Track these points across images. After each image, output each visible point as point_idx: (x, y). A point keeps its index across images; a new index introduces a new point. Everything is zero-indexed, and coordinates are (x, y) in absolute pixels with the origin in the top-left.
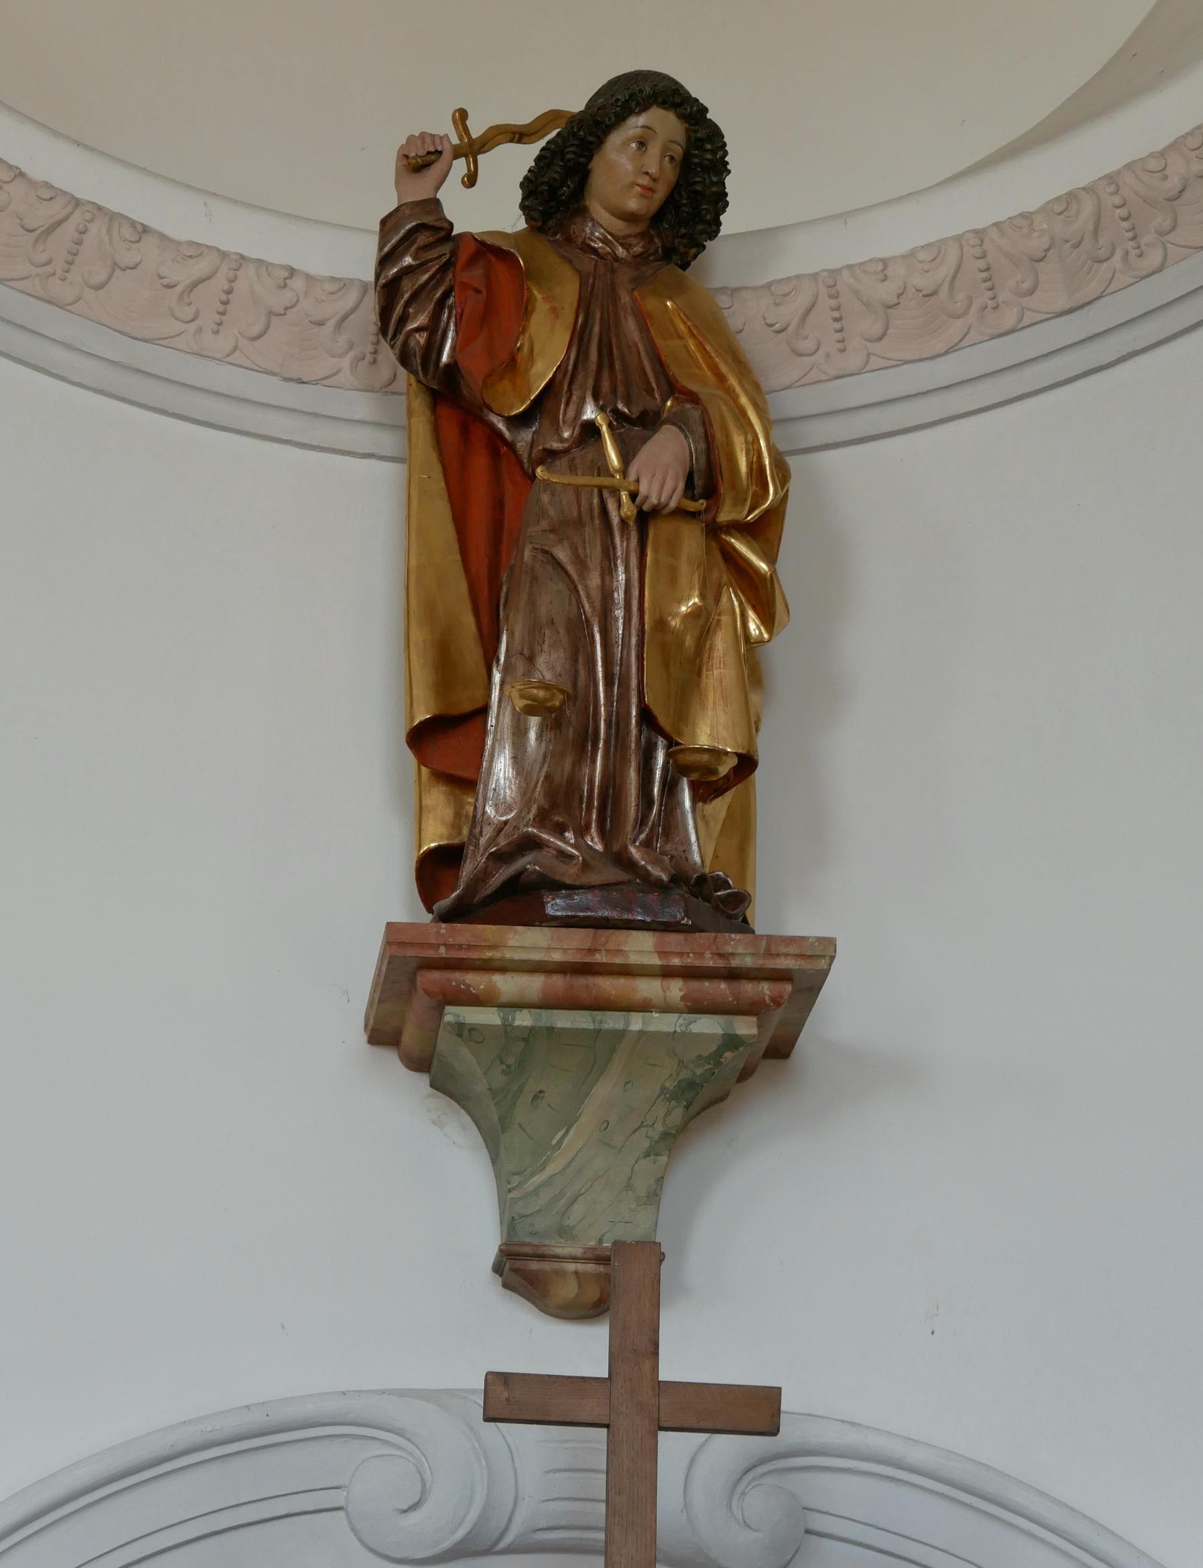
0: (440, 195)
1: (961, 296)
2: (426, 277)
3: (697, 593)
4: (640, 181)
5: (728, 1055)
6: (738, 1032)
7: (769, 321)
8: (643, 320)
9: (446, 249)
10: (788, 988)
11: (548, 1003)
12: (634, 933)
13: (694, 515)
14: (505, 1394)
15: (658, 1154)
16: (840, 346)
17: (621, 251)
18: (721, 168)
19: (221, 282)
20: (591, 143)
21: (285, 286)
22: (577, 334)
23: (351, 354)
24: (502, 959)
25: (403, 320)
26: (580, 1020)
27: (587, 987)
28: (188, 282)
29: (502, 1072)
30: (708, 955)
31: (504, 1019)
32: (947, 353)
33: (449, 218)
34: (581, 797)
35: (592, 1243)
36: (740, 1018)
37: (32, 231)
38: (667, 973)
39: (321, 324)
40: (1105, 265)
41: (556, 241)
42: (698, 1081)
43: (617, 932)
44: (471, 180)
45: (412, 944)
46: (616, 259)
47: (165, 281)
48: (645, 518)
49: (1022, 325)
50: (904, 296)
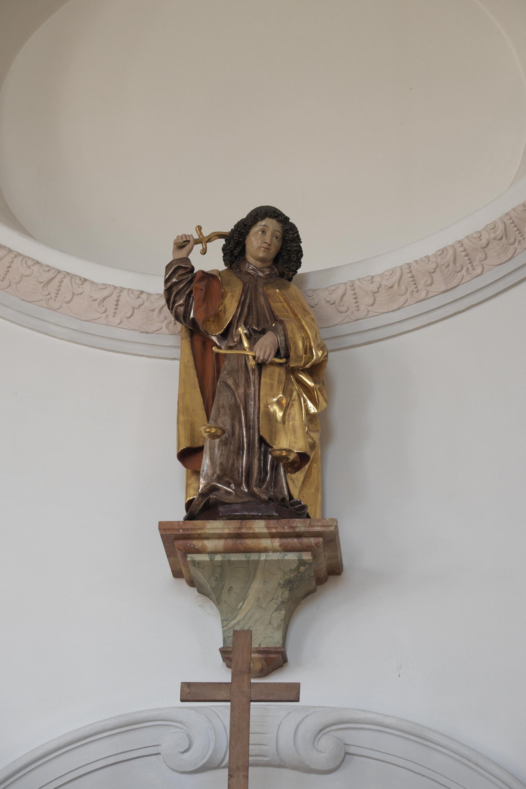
0: (189, 257)
1: (403, 288)
2: (182, 285)
3: (281, 393)
4: (263, 246)
5: (302, 568)
6: (304, 558)
7: (328, 300)
8: (266, 297)
9: (190, 276)
10: (321, 539)
11: (227, 551)
12: (257, 521)
13: (281, 364)
14: (188, 691)
15: (281, 610)
16: (357, 308)
17: (260, 274)
18: (298, 240)
19: (114, 297)
20: (243, 233)
21: (139, 297)
22: (241, 303)
23: (166, 321)
24: (205, 533)
25: (174, 303)
26: (241, 557)
27: (241, 543)
28: (101, 298)
29: (215, 580)
30: (286, 527)
31: (211, 558)
32: (399, 309)
33: (193, 264)
34: (239, 472)
35: (257, 646)
36: (304, 553)
37: (42, 283)
38: (273, 536)
39: (153, 310)
40: (459, 273)
41: (236, 272)
42: (292, 579)
43: (250, 521)
44: (204, 252)
45: (169, 529)
46: (259, 276)
47: (93, 298)
48: (261, 366)
49: (428, 297)
50: (380, 288)
